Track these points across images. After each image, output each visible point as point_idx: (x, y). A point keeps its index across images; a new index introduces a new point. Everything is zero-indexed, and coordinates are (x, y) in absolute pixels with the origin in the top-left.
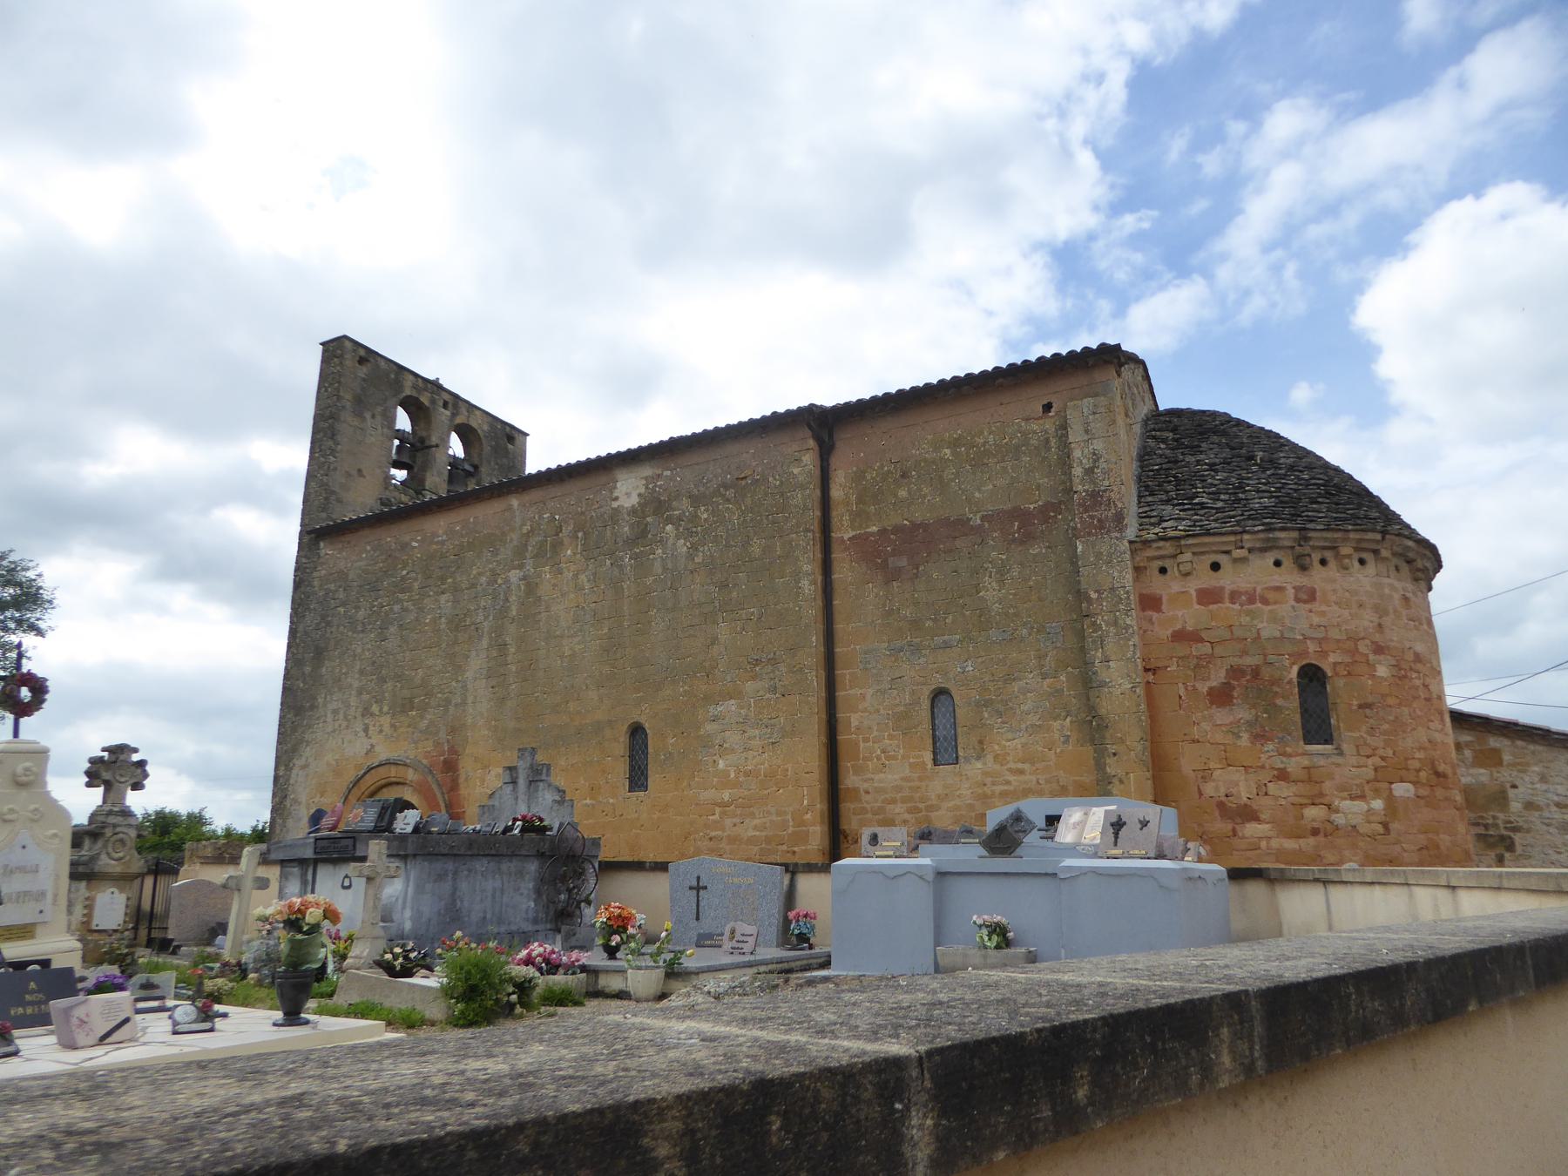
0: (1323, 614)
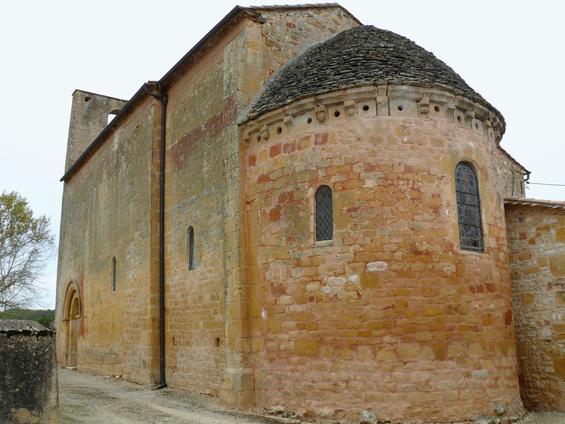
0: (330, 150)
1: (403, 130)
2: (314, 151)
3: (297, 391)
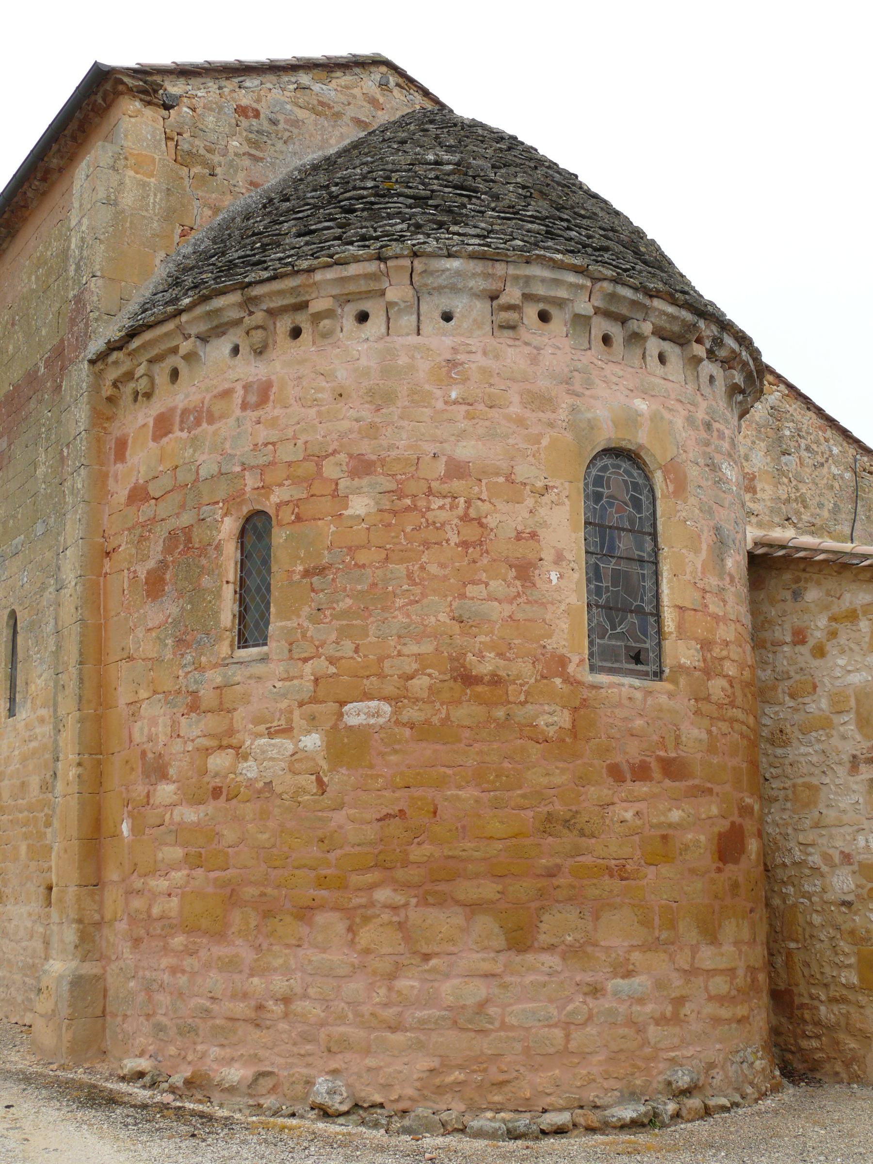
0: (273, 423)
1: (449, 372)
2: (239, 426)
3: (179, 1021)
